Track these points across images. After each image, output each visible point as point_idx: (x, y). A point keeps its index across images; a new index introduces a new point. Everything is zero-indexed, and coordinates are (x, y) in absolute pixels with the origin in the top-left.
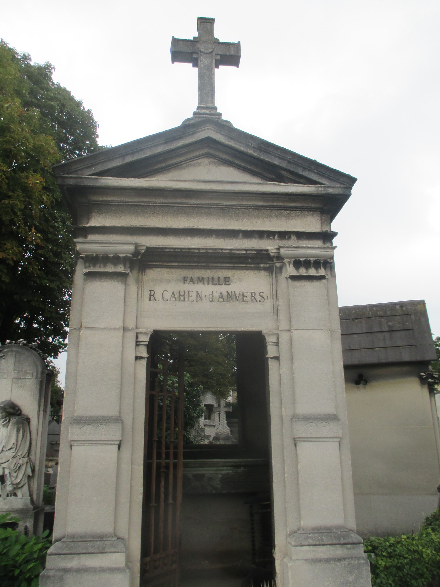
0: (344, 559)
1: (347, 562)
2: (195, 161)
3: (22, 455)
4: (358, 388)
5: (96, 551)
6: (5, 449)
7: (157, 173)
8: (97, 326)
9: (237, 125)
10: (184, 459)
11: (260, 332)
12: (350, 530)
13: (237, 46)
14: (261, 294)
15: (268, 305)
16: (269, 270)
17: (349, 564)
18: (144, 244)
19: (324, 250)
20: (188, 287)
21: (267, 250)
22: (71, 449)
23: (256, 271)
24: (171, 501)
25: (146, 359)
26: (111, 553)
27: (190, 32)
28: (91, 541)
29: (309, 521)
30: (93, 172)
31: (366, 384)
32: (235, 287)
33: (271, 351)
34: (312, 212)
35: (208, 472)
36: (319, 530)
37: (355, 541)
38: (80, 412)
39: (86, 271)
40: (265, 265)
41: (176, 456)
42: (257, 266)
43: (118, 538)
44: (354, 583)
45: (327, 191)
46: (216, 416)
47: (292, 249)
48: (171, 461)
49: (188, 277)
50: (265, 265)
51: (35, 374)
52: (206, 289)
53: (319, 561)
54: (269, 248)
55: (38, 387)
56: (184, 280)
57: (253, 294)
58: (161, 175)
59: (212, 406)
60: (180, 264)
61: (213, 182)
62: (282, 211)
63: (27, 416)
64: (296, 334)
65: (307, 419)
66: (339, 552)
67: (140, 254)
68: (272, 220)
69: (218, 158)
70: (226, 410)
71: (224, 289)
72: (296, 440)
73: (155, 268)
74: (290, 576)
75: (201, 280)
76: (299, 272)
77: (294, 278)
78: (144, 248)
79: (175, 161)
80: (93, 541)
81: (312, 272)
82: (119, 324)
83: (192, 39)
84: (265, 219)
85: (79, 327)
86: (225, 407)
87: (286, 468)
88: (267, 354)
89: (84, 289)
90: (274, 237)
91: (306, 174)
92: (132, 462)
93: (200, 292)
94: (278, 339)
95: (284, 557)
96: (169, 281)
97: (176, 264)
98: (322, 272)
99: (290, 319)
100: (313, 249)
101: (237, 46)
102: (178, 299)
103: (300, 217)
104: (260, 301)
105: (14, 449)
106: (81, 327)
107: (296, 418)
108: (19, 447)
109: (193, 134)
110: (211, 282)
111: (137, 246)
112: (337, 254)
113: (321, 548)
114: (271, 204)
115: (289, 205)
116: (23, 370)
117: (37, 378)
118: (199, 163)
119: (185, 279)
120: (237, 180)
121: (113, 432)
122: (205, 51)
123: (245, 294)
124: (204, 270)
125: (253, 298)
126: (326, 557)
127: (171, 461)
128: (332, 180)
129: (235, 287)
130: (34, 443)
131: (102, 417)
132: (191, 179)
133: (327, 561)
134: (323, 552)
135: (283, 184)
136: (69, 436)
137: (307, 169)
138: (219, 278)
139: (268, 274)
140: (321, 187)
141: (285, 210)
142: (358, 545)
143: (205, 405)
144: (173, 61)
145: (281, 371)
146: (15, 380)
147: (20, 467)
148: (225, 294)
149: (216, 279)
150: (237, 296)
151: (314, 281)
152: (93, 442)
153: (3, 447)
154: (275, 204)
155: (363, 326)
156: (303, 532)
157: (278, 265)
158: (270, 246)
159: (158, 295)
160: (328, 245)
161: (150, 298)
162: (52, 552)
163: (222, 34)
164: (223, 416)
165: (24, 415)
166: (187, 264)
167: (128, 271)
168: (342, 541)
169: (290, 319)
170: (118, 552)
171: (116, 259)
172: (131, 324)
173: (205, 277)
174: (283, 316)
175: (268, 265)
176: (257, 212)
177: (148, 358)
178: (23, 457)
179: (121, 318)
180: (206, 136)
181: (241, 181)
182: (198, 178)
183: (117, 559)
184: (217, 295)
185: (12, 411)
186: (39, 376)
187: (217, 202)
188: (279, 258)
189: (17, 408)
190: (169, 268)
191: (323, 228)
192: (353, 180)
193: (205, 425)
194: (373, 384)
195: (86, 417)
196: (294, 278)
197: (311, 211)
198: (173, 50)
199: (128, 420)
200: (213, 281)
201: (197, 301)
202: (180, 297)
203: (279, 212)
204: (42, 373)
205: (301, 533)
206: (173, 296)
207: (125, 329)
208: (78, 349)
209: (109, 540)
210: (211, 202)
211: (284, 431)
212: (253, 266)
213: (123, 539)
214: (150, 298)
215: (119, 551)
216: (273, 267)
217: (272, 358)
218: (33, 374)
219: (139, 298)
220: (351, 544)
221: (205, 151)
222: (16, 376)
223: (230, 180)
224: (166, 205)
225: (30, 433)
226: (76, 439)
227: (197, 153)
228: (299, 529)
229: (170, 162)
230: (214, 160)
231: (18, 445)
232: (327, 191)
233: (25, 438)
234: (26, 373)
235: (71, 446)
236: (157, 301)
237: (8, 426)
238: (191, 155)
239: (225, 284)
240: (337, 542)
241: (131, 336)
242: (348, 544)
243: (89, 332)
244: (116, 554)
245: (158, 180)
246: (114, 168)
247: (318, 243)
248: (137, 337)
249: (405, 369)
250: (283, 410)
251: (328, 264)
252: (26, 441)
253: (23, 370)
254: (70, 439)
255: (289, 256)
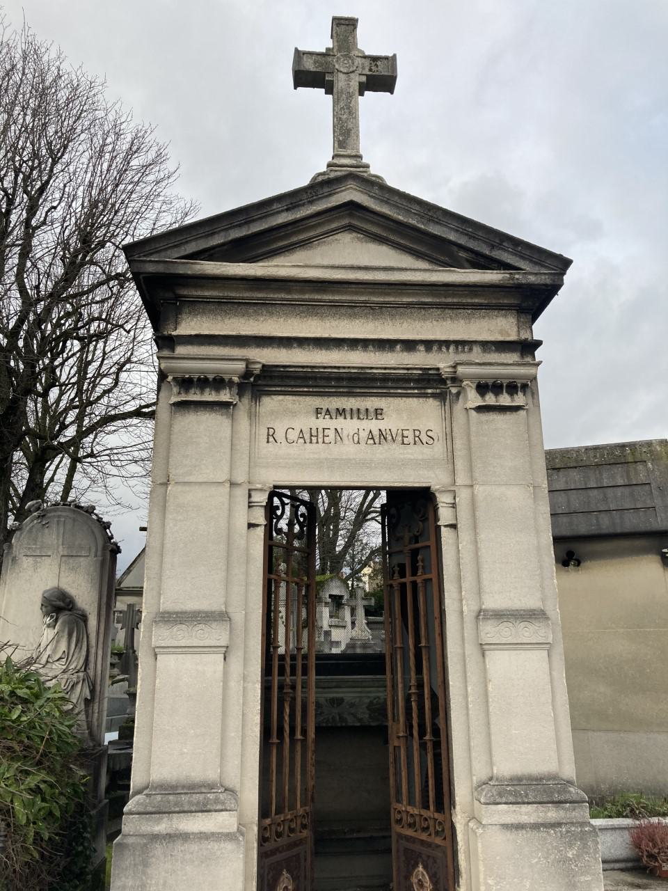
0: (559, 824)
1: (564, 830)
2: (331, 237)
3: (75, 668)
4: (568, 571)
5: (193, 809)
6: (50, 660)
7: (276, 255)
8: (192, 479)
9: (391, 182)
10: (302, 675)
11: (428, 488)
12: (567, 782)
13: (391, 61)
14: (429, 433)
15: (439, 449)
16: (441, 397)
17: (568, 832)
18: (258, 360)
19: (522, 368)
20: (324, 422)
21: (438, 369)
22: (156, 659)
23: (421, 400)
24: (299, 736)
25: (263, 528)
26: (216, 811)
27: (321, 41)
28: (186, 794)
29: (506, 767)
30: (183, 254)
31: (578, 565)
32: (389, 423)
33: (445, 515)
34: (503, 312)
35: (348, 695)
36: (517, 780)
37: (575, 798)
38: (167, 604)
39: (174, 399)
40: (434, 391)
41: (305, 671)
42: (423, 391)
43: (226, 790)
44: (575, 861)
45: (524, 280)
46: (347, 613)
47: (477, 366)
48: (299, 678)
49: (322, 409)
50: (434, 391)
51: (93, 550)
52: (349, 426)
53: (519, 827)
54: (441, 365)
55: (98, 570)
56: (318, 413)
57: (417, 433)
58: (282, 258)
59: (341, 597)
60: (311, 390)
61: (360, 268)
62: (460, 311)
63: (83, 611)
64: (478, 489)
65: (500, 616)
66: (552, 814)
67: (253, 374)
68: (444, 323)
69: (364, 231)
70: (365, 603)
71: (374, 425)
72: (484, 647)
73: (275, 395)
74: (480, 850)
75: (341, 412)
76: (485, 401)
77: (480, 409)
78: (259, 366)
79: (302, 237)
80: (191, 793)
81: (505, 400)
82: (223, 476)
83: (324, 51)
84: (435, 323)
85: (165, 481)
86: (363, 599)
87: (469, 689)
88: (439, 520)
89: (171, 426)
90: (448, 349)
91: (497, 254)
92: (245, 678)
93: (340, 431)
94: (455, 498)
95: (469, 821)
96: (294, 414)
97: (306, 389)
98: (520, 399)
99: (471, 470)
100: (507, 366)
101: (391, 61)
102: (308, 441)
103: (487, 318)
104: (427, 443)
105: (64, 660)
106: (168, 481)
107: (482, 615)
108: (72, 657)
109: (330, 195)
110: (355, 416)
111: (248, 362)
112: (541, 373)
113: (525, 808)
114: (443, 300)
115: (469, 301)
116: (77, 543)
117: (96, 556)
118: (336, 240)
119: (318, 411)
120: (393, 264)
121: (216, 635)
122: (342, 70)
123: (405, 432)
124: (346, 398)
125: (417, 439)
126: (532, 822)
127: (299, 678)
128: (536, 263)
129: (389, 423)
130: (93, 651)
131: (199, 612)
132: (325, 263)
133: (536, 827)
134: (527, 814)
135: (463, 270)
136: (153, 640)
137: (497, 247)
138: (367, 409)
139: (438, 403)
140: (518, 274)
141: (464, 309)
142: (580, 804)
143: (331, 596)
144: (296, 86)
145: (460, 546)
146: (64, 559)
147: (73, 686)
148: (376, 433)
149: (363, 410)
150: (394, 436)
151: (508, 413)
152: (186, 649)
153: (49, 656)
154: (449, 300)
155: (576, 478)
156: (496, 784)
157: (454, 390)
158: (442, 362)
159: (280, 435)
160: (529, 359)
161: (268, 438)
162: (130, 810)
163: (369, 42)
164: (361, 612)
165: (79, 609)
166: (322, 390)
167: (235, 400)
168: (556, 797)
169: (471, 470)
170: (227, 810)
171: (219, 383)
172: (241, 477)
173: (348, 409)
174: (460, 464)
175: (438, 391)
176: (423, 312)
177: (265, 526)
178: (77, 672)
179: (226, 469)
180: (347, 199)
181: (400, 265)
182: (337, 263)
183: (223, 821)
184: (364, 435)
185: (62, 604)
186: (99, 553)
187: (363, 298)
188: (456, 380)
189: (68, 600)
190: (295, 395)
191: (521, 334)
192: (565, 263)
193: (330, 626)
194: (587, 564)
195: (177, 613)
196: (480, 409)
197: (503, 310)
198: (297, 69)
199: (238, 617)
200: (357, 414)
201: (335, 443)
202: (312, 436)
203: (455, 311)
204: (104, 548)
205: (494, 785)
206: (301, 436)
207: (233, 484)
208: (164, 513)
209: (214, 793)
210: (355, 298)
211: (466, 634)
212: (416, 391)
213: (232, 791)
214: (268, 438)
215: (228, 808)
216: (446, 392)
217: (446, 526)
218: (90, 549)
219: (253, 438)
220: (570, 802)
221: (346, 221)
222: (66, 553)
223: (384, 264)
224: (289, 302)
225: (88, 637)
226: (162, 645)
227: (334, 226)
228: (491, 779)
229: (294, 239)
230: (359, 235)
231: (71, 654)
232: (524, 280)
233: (79, 645)
234: (81, 547)
235: (156, 655)
236: (279, 444)
237: (55, 626)
238: (325, 228)
239: (377, 419)
240: (549, 799)
241: (241, 494)
242: (566, 802)
243: (180, 488)
244: (223, 813)
245: (277, 266)
246: (213, 248)
247: (513, 357)
248: (250, 496)
249: (638, 543)
250: (464, 602)
251: (525, 386)
252: (81, 648)
253: (77, 543)
254: (153, 644)
255: (471, 377)
